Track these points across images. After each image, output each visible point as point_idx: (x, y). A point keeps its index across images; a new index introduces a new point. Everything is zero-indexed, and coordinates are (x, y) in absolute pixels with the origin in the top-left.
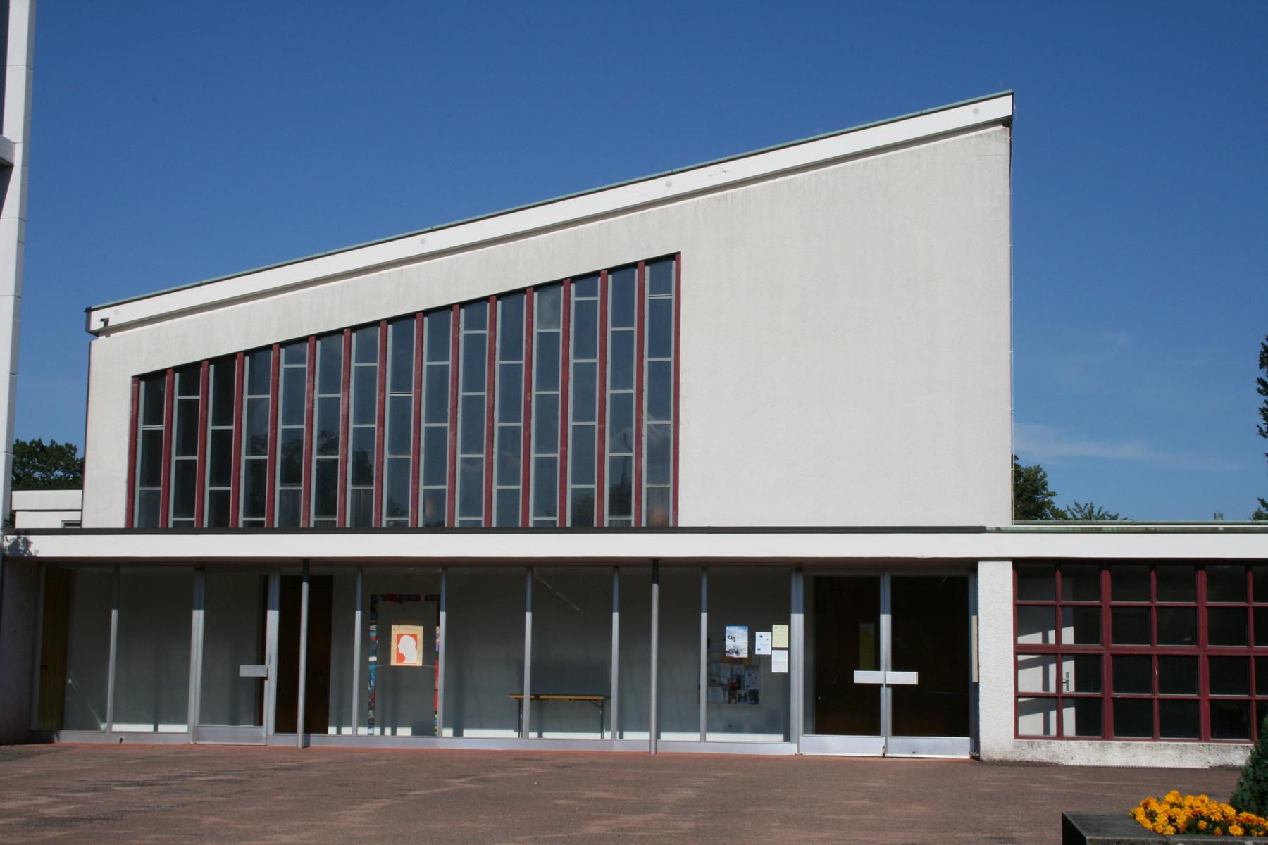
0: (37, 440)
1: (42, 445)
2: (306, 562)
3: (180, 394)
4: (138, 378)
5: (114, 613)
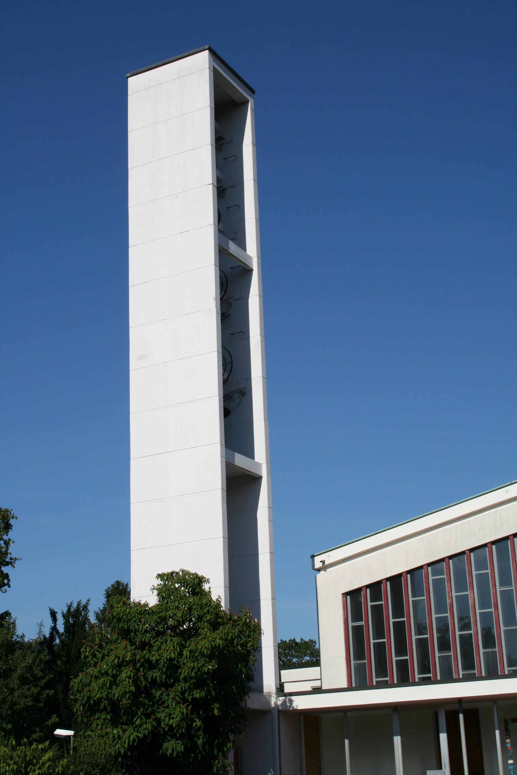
0: (292, 639)
1: (296, 642)
2: (460, 701)
3: (371, 602)
4: (345, 594)
5: (347, 741)
